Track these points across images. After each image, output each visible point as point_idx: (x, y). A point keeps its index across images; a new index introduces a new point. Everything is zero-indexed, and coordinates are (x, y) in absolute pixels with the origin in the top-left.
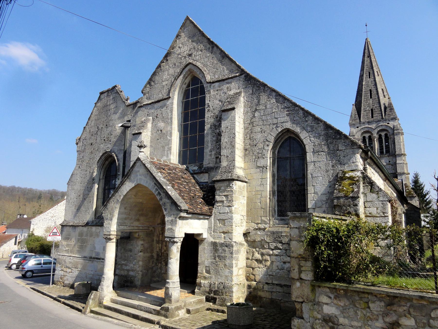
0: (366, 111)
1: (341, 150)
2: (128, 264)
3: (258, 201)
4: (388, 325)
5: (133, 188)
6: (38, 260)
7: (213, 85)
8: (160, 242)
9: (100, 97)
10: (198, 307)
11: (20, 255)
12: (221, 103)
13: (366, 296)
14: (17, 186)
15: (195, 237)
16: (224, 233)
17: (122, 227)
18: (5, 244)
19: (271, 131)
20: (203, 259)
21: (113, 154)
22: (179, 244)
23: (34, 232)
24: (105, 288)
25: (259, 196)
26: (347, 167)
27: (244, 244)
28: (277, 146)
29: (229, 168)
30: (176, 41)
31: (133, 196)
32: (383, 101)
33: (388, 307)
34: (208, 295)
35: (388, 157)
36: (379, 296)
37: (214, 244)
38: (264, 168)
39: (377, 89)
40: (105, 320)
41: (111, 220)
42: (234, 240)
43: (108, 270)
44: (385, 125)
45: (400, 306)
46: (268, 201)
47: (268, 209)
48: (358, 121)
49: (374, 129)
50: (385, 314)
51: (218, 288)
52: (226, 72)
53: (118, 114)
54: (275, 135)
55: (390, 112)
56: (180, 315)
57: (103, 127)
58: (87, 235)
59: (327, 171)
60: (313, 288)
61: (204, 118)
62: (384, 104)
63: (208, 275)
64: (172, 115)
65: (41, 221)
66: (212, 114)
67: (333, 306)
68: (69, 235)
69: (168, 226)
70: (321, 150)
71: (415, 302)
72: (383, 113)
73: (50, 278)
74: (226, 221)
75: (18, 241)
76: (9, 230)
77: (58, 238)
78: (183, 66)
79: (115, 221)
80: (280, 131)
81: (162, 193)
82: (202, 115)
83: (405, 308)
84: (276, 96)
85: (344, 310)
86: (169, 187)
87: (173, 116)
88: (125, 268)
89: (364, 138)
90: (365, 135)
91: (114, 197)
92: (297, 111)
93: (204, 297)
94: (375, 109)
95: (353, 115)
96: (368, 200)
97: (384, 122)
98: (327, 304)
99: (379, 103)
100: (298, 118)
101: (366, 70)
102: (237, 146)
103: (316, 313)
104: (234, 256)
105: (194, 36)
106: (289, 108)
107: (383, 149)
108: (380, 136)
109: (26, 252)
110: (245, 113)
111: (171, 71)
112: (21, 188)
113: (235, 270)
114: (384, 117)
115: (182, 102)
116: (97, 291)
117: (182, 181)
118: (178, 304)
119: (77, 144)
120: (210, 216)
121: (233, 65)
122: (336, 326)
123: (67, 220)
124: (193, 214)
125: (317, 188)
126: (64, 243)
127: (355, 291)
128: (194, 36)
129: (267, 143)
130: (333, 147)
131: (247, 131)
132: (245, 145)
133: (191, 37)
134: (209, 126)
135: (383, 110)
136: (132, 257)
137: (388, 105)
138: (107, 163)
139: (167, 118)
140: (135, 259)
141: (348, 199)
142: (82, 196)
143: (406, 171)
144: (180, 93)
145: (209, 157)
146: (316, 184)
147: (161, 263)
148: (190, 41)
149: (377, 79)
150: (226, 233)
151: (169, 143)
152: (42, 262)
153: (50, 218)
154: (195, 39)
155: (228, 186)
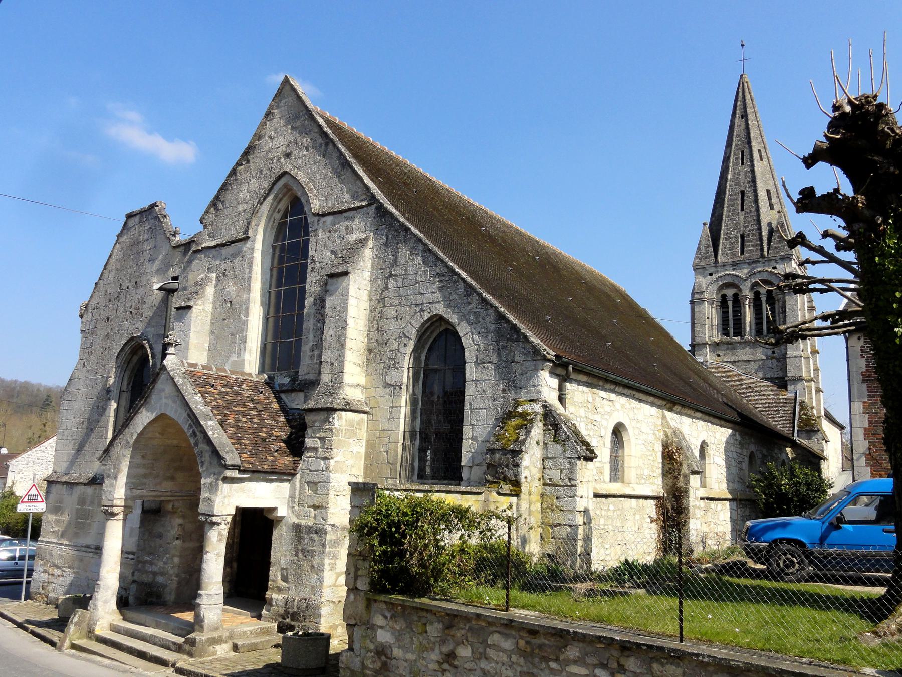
0: (729, 238)
1: (517, 362)
2: (156, 561)
3: (384, 449)
4: (444, 656)
9: (125, 224)
10: (257, 641)
13: (424, 614)
16: (315, 507)
17: (138, 492)
21: (145, 342)
23: (14, 489)
24: (100, 604)
25: (386, 440)
28: (423, 347)
31: (157, 435)
34: (281, 620)
37: (297, 528)
39: (755, 191)
40: (94, 662)
41: (116, 478)
42: (330, 521)
43: (108, 572)
47: (399, 464)
48: (712, 259)
50: (443, 642)
52: (347, 196)
53: (157, 263)
54: (418, 326)
58: (92, 503)
59: (494, 400)
60: (369, 603)
62: (770, 224)
63: (284, 584)
64: (250, 272)
65: (31, 464)
66: (319, 278)
69: (204, 495)
70: (488, 359)
71: (473, 623)
72: (765, 245)
73: (21, 589)
77: (41, 507)
78: (274, 176)
79: (122, 479)
80: (426, 318)
81: (198, 434)
82: (303, 279)
83: (463, 632)
85: (399, 636)
86: (210, 423)
87: (253, 275)
89: (724, 297)
90: (724, 292)
93: (275, 625)
95: (703, 248)
96: (549, 456)
97: (766, 264)
98: (382, 627)
100: (456, 297)
101: (736, 146)
102: (349, 344)
104: (327, 550)
105: (297, 117)
107: (762, 323)
108: (757, 295)
110: (373, 280)
111: (254, 184)
114: (765, 253)
115: (274, 248)
116: (87, 609)
117: (250, 409)
118: (216, 635)
119: (81, 316)
121: (359, 183)
122: (389, 661)
123: (59, 470)
124: (253, 472)
125: (476, 430)
126: (51, 517)
129: (405, 340)
131: (373, 315)
132: (369, 342)
133: (291, 120)
135: (765, 238)
136: (162, 549)
138: (135, 358)
139: (243, 279)
140: (167, 552)
141: (505, 455)
142: (86, 423)
144: (269, 229)
145: (309, 362)
146: (475, 423)
148: (289, 127)
149: (759, 167)
150: (318, 507)
151: (242, 327)
154: (298, 124)
155: (326, 420)
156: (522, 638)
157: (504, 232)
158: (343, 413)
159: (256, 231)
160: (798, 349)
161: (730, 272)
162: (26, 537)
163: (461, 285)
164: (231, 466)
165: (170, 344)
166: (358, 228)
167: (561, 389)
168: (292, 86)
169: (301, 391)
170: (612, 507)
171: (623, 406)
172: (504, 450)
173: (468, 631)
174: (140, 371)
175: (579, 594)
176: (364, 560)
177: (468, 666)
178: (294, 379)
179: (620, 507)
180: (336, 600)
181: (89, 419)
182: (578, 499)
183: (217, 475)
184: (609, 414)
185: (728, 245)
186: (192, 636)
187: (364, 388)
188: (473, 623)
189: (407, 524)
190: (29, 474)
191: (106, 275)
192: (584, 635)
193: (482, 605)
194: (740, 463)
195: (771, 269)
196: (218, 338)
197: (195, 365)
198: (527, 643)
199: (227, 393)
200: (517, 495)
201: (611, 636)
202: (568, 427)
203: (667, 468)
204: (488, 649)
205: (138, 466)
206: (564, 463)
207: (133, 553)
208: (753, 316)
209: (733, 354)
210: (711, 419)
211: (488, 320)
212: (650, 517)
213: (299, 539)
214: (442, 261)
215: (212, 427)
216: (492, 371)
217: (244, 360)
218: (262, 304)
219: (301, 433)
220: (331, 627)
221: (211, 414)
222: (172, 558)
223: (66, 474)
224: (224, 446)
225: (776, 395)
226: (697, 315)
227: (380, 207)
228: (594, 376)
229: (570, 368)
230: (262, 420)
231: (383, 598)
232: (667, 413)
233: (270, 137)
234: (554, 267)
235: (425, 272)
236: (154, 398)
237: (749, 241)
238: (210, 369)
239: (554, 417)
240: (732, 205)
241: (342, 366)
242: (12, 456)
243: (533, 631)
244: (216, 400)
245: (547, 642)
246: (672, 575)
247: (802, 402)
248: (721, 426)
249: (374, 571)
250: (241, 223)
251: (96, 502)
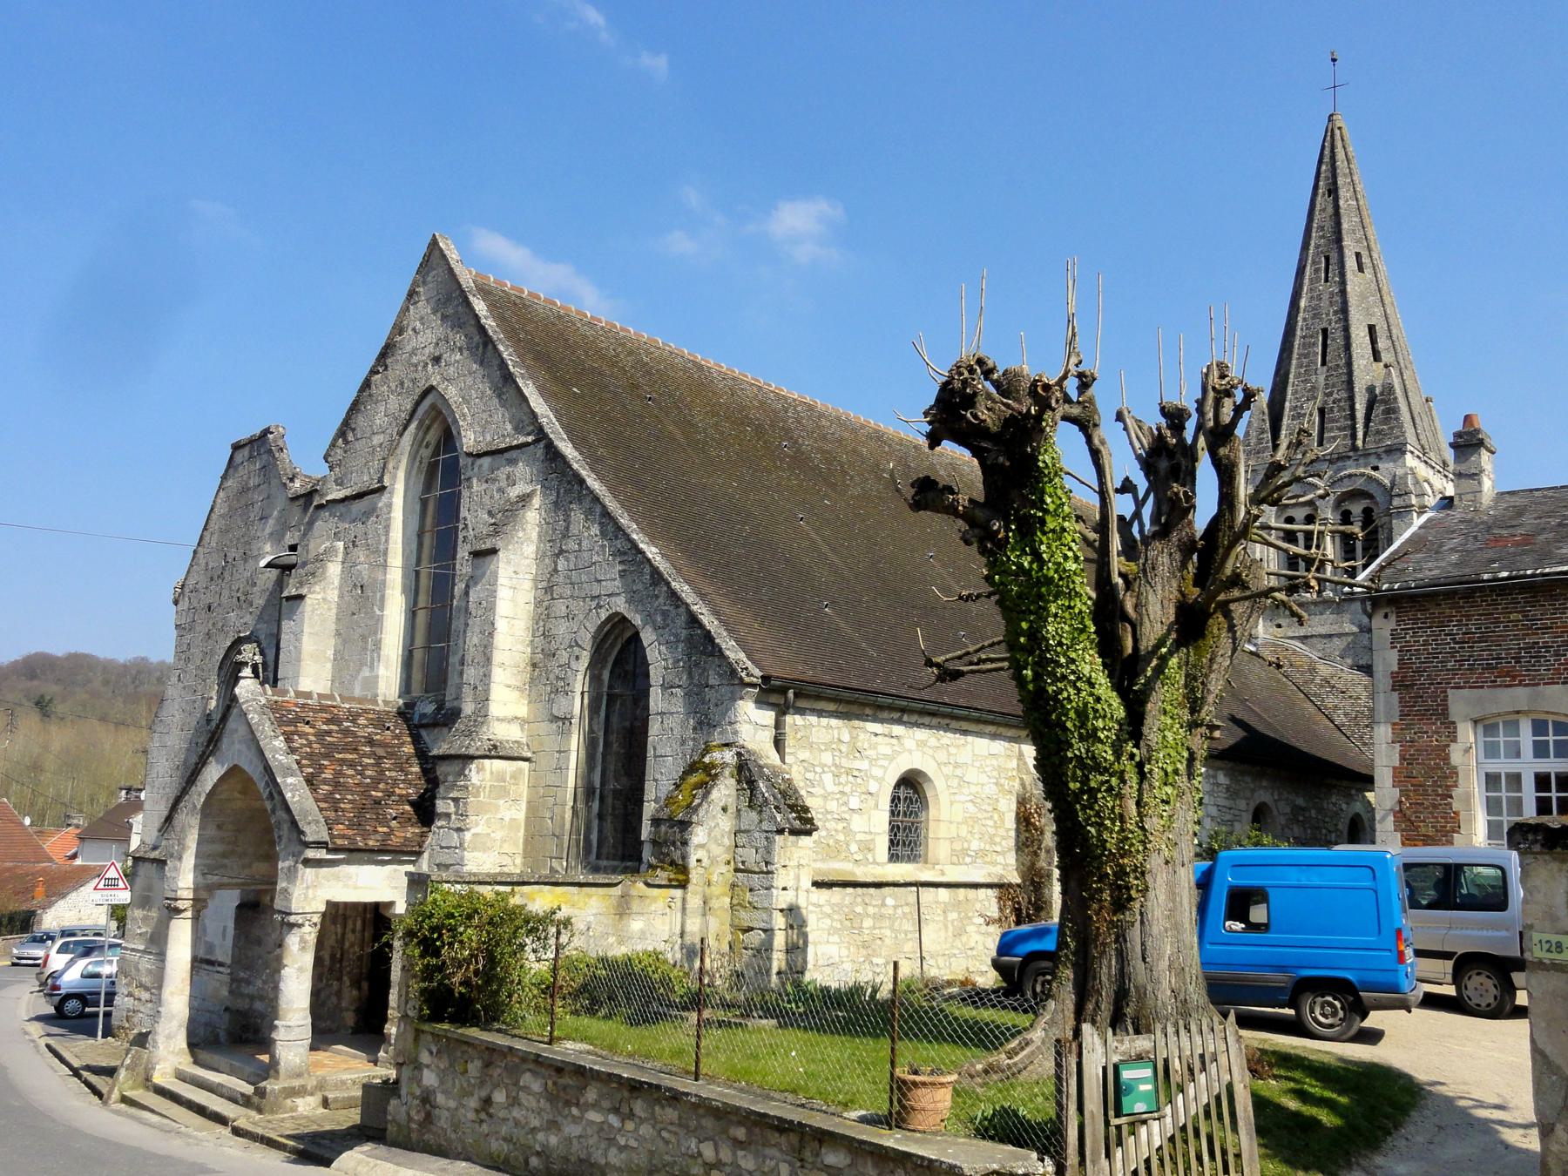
1: (712, 687)
3: (548, 815)
8: (340, 920)
11: (76, 943)
15: (382, 911)
18: (61, 903)
22: (310, 933)
31: (237, 795)
32: (1366, 373)
39: (1346, 329)
41: (180, 858)
44: (1363, 475)
46: (568, 815)
50: (482, 1084)
52: (509, 427)
53: (271, 522)
55: (1386, 421)
59: (683, 743)
62: (1371, 389)
69: (281, 884)
70: (677, 681)
76: (90, 847)
78: (418, 391)
85: (442, 1075)
86: (290, 780)
94: (1332, 410)
95: (1253, 434)
98: (428, 1066)
101: (1317, 246)
102: (497, 657)
105: (448, 300)
110: (540, 557)
114: (1359, 443)
115: (424, 503)
117: (365, 755)
118: (296, 1083)
119: (176, 602)
120: (419, 854)
124: (351, 851)
126: (138, 913)
139: (377, 551)
144: (414, 472)
147: (340, 979)
149: (1356, 284)
151: (376, 625)
156: (550, 1077)
158: (487, 762)
159: (394, 477)
167: (778, 725)
168: (441, 250)
177: (502, 1114)
178: (440, 707)
183: (296, 855)
184: (891, 758)
187: (523, 722)
191: (207, 539)
198: (555, 1083)
199: (329, 733)
200: (683, 885)
203: (1023, 837)
205: (212, 841)
215: (294, 789)
218: (405, 590)
221: (295, 766)
224: (306, 813)
228: (849, 702)
229: (791, 694)
230: (382, 772)
233: (414, 330)
235: (603, 546)
237: (1333, 421)
240: (1306, 356)
241: (487, 691)
244: (309, 745)
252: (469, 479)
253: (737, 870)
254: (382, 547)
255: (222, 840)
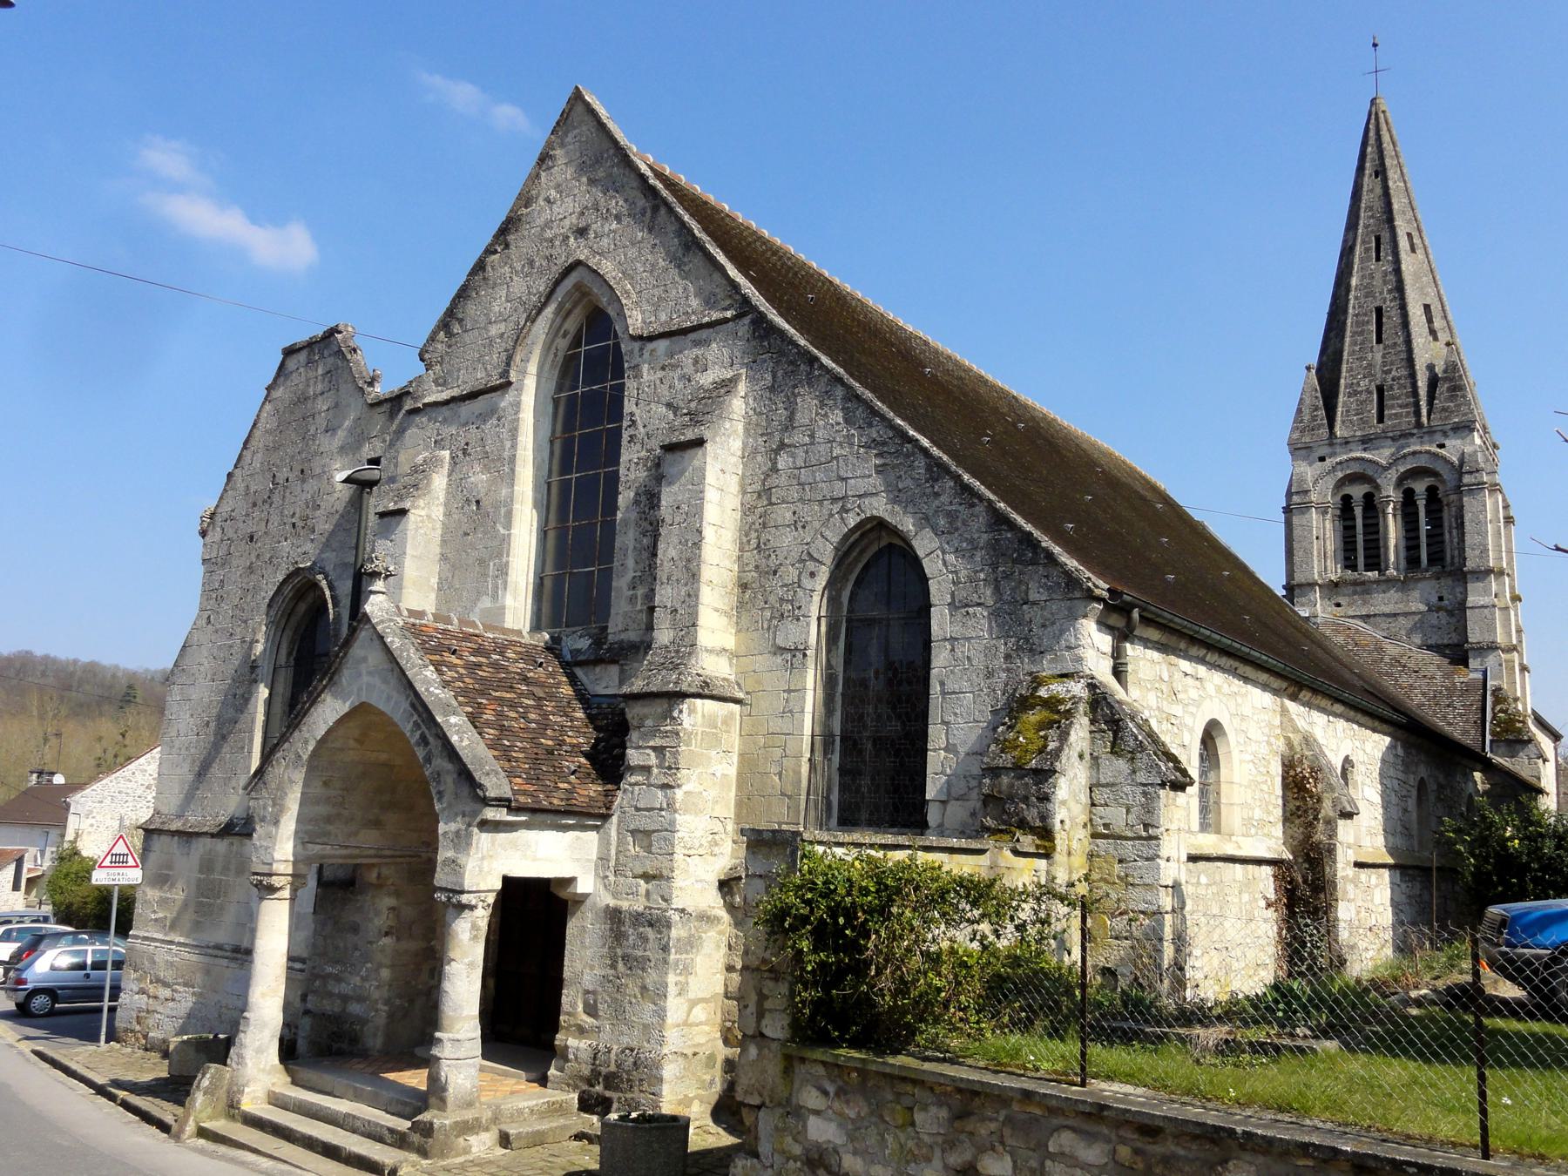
1: (1034, 603)
3: (774, 769)
5: (347, 715)
6: (77, 953)
7: (650, 346)
10: (544, 1126)
12: (671, 416)
13: (909, 1088)
14: (39, 652)
16: (647, 877)
17: (316, 849)
19: (825, 524)
20: (578, 966)
21: (320, 577)
22: (481, 917)
23: (80, 845)
24: (249, 1053)
25: (779, 752)
26: (1050, 662)
27: (718, 919)
29: (677, 652)
30: (538, 176)
31: (352, 743)
32: (1427, 352)
33: (957, 1124)
34: (585, 1087)
35: (1434, 582)
36: (938, 1090)
37: (614, 916)
38: (796, 653)
39: (1403, 307)
40: (232, 1160)
41: (276, 823)
42: (677, 903)
43: (263, 995)
44: (1428, 452)
45: (983, 1119)
46: (805, 769)
47: (803, 797)
48: (1324, 432)
49: (1386, 469)
50: (950, 1144)
51: (618, 1066)
52: (695, 303)
53: (341, 434)
54: (836, 540)
55: (1452, 398)
56: (474, 1150)
57: (292, 477)
60: (790, 1064)
61: (618, 464)
62: (1431, 367)
63: (590, 1020)
64: (514, 446)
66: (644, 453)
67: (831, 1120)
68: (170, 867)
69: (444, 853)
70: (975, 598)
72: (1423, 403)
74: (653, 836)
75: (25, 876)
77: (133, 876)
78: (556, 271)
80: (852, 523)
81: (431, 739)
82: (614, 456)
83: (993, 1126)
84: (846, 399)
85: (854, 1131)
86: (453, 720)
87: (520, 453)
88: (336, 989)
89: (1347, 499)
90: (1348, 490)
91: (286, 745)
92: (907, 456)
94: (1391, 388)
95: (1306, 411)
96: (1103, 781)
97: (1426, 438)
98: (817, 1113)
99: (1410, 362)
100: (909, 483)
101: (1366, 227)
102: (707, 573)
103: (789, 1139)
104: (672, 957)
105: (598, 161)
106: (884, 444)
107: (1418, 547)
108: (1409, 497)
109: (46, 920)
110: (748, 455)
111: (519, 286)
112: (54, 661)
113: (675, 1007)
114: (1424, 420)
115: (556, 402)
116: (225, 1064)
117: (521, 695)
118: (469, 1115)
119: (203, 534)
120: (605, 817)
121: (717, 276)
123: (164, 810)
124: (533, 811)
125: (955, 732)
126: (152, 894)
127: (885, 1075)
128: (597, 161)
129: (811, 565)
130: (1013, 589)
131: (750, 519)
134: (632, 494)
136: (357, 953)
137: (1445, 371)
138: (302, 607)
140: (367, 958)
141: (1022, 778)
142: (213, 725)
143: (1500, 639)
144: (547, 367)
146: (952, 719)
148: (584, 179)
149: (1408, 264)
150: (654, 877)
151: (501, 547)
152: (89, 962)
153: (139, 792)
154: (601, 174)
155: (667, 715)
156: (1123, 1141)
157: (961, 378)
158: (698, 701)
159: (524, 372)
160: (1487, 592)
161: (1358, 455)
162: (108, 929)
163: (920, 463)
164: (496, 799)
165: (375, 575)
166: (718, 361)
168: (588, 105)
169: (613, 662)
170: (1203, 880)
171: (1218, 689)
172: (1018, 769)
173: (1004, 1123)
174: (312, 631)
175: (1205, 1049)
176: (776, 980)
178: (599, 640)
179: (1217, 878)
180: (689, 1052)
181: (219, 717)
182: (1162, 863)
184: (1197, 703)
185: (1354, 406)
186: (425, 1117)
187: (734, 655)
188: (1016, 1107)
189: (870, 911)
190: (107, 818)
192: (1270, 1141)
193: (1024, 1071)
194: (1403, 798)
195: (1434, 449)
196: (459, 564)
197: (420, 614)
198: (1137, 1152)
199: (479, 665)
200: (1047, 856)
201: (1328, 1142)
202: (1139, 727)
203: (1291, 806)
204: (1048, 1163)
206: (1134, 796)
207: (303, 961)
208: (1402, 533)
209: (1365, 603)
210: (1359, 716)
211: (974, 525)
212: (1265, 898)
213: (618, 936)
214: (883, 418)
216: (985, 622)
217: (504, 608)
218: (536, 505)
219: (615, 740)
220: (680, 1103)
221: (455, 703)
222: (377, 971)
223: (179, 817)
225: (1447, 676)
226: (1297, 532)
227: (760, 320)
229: (1136, 614)
230: (545, 715)
231: (818, 1054)
232: (1288, 703)
233: (548, 200)
234: (1050, 443)
236: (346, 676)
237: (1393, 398)
238: (448, 621)
239: (1111, 707)
240: (1361, 333)
242: (74, 787)
243: (1149, 1129)
245: (1181, 1152)
246: (1312, 999)
247: (1498, 689)
248: (1374, 730)
249: (802, 1002)
250: (495, 358)
251: (232, 867)
252: (636, 367)
253: (1095, 836)
254: (506, 454)
255: (328, 800)
